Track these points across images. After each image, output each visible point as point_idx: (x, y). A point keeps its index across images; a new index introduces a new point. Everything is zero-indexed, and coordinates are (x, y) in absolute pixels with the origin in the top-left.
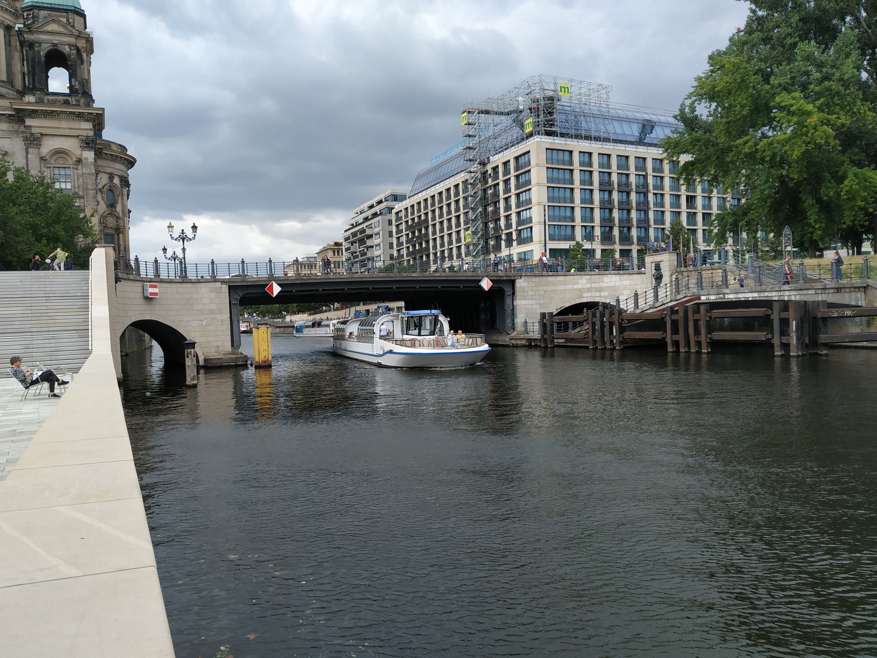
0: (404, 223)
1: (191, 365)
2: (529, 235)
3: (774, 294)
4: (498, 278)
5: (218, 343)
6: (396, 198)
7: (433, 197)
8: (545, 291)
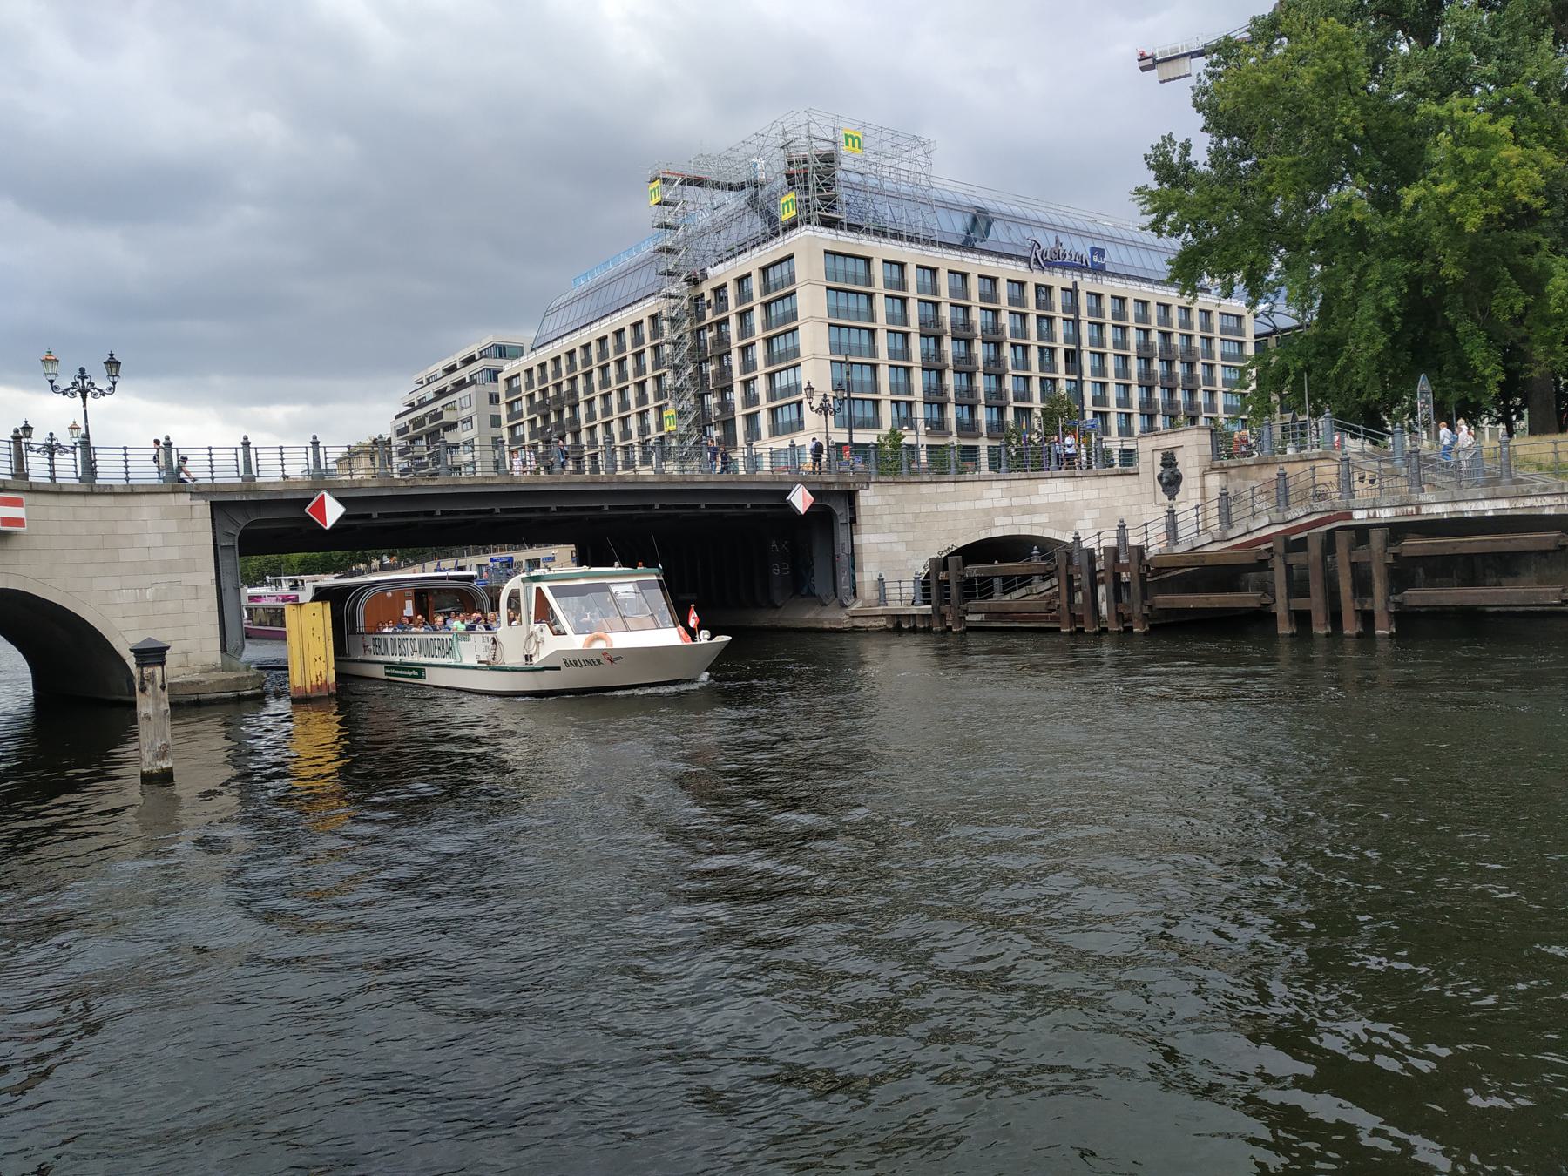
1: (155, 715)
2: (795, 417)
3: (1548, 501)
5: (186, 645)
6: (503, 352)
7: (556, 360)
8: (916, 515)
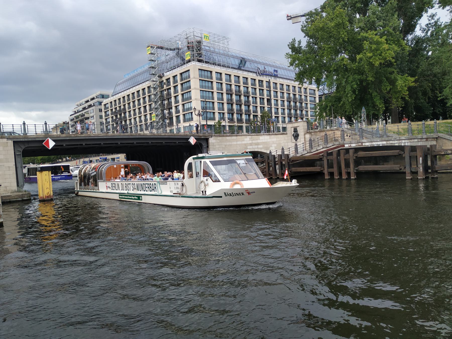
0: (110, 111)
2: (190, 117)
3: (396, 142)
4: (199, 137)
8: (226, 145)
